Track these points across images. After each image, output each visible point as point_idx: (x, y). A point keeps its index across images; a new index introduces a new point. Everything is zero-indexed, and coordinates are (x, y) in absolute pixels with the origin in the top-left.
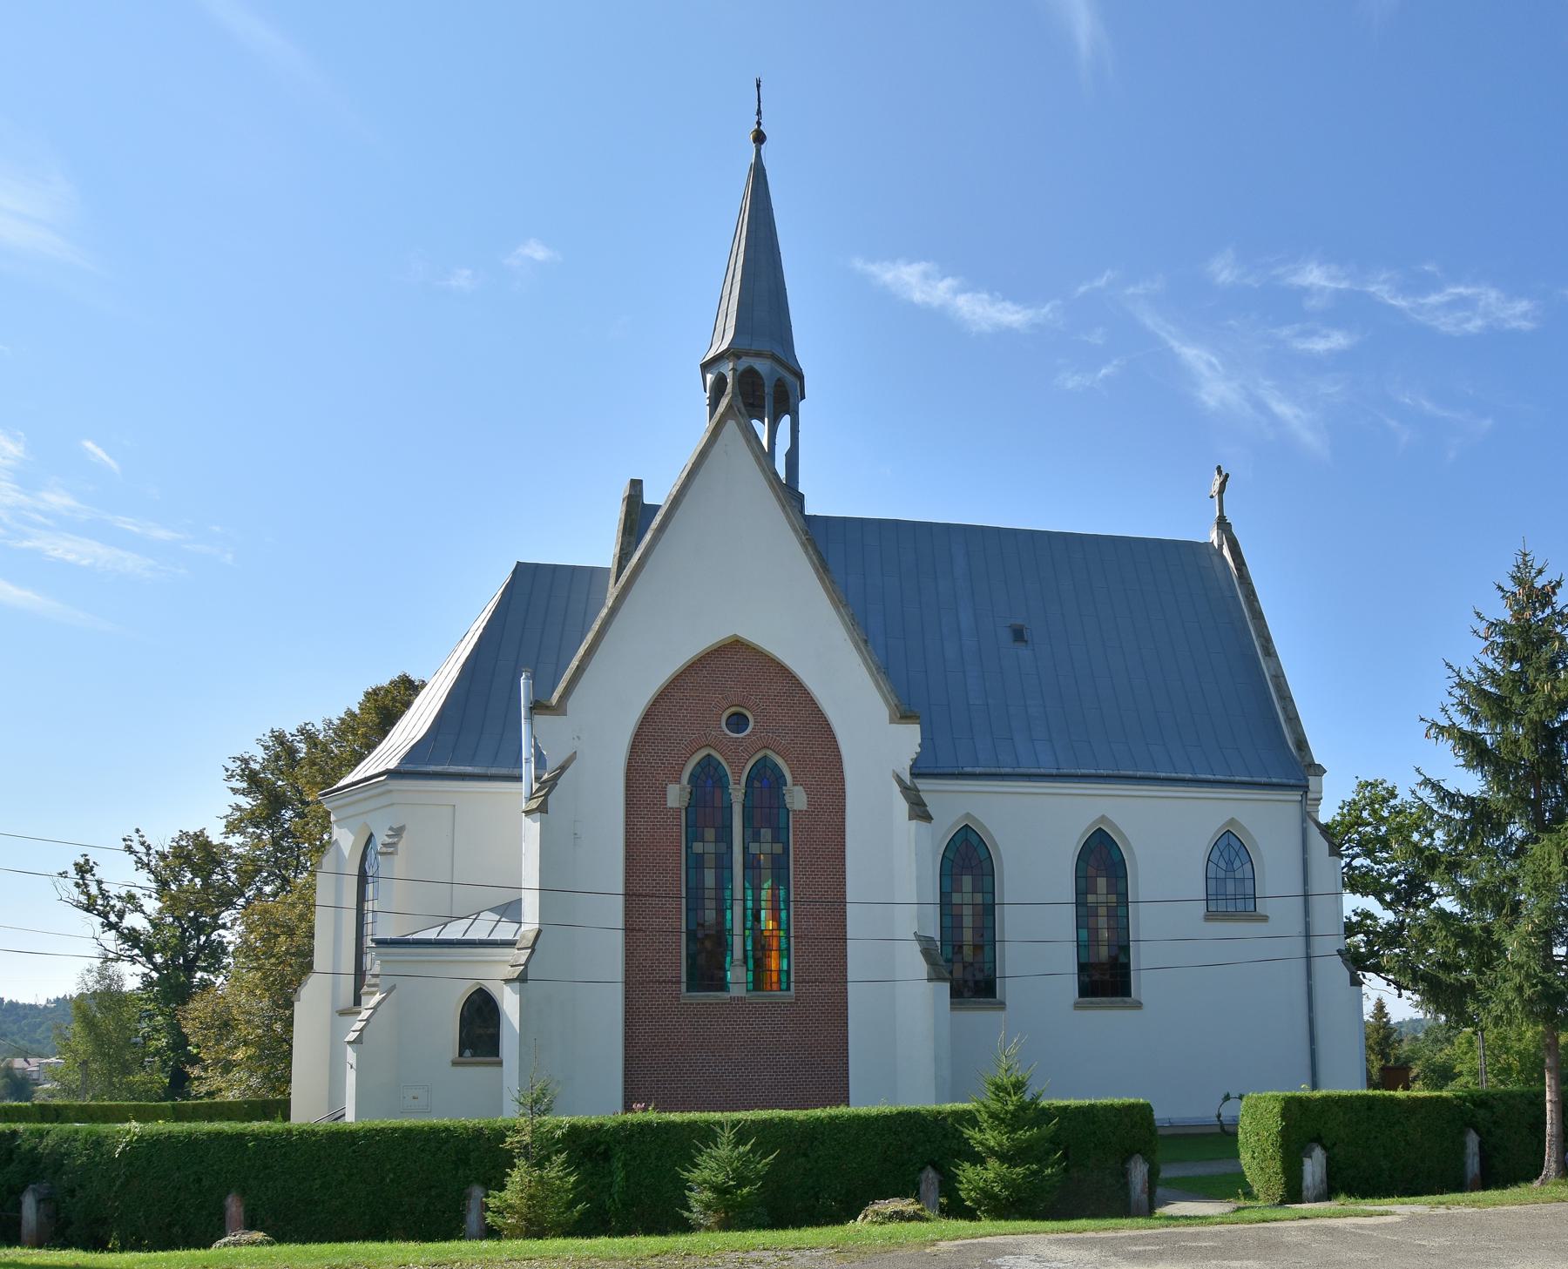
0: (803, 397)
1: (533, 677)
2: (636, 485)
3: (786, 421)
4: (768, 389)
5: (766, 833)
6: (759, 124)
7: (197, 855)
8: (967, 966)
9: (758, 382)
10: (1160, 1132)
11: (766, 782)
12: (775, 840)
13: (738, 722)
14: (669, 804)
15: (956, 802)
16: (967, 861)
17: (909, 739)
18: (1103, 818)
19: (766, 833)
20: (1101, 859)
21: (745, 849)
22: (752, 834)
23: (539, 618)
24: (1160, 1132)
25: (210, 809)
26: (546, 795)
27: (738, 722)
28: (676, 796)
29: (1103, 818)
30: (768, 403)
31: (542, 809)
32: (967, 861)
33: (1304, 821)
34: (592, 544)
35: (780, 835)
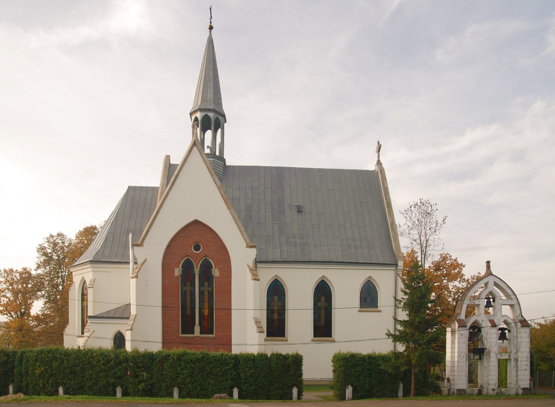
0: (226, 122)
2: (168, 158)
3: (220, 130)
4: (213, 120)
5: (206, 284)
6: (211, 22)
7: (26, 276)
8: (276, 327)
9: (210, 118)
11: (206, 268)
12: (209, 286)
13: (197, 248)
14: (176, 275)
15: (268, 274)
16: (276, 292)
17: (253, 253)
18: (324, 276)
19: (206, 284)
20: (323, 292)
21: (200, 289)
22: (201, 285)
23: (138, 206)
24: (305, 383)
25: (29, 260)
26: (138, 272)
27: (197, 248)
28: (178, 272)
29: (324, 276)
32: (276, 292)
33: (396, 277)
34: (154, 179)
35: (210, 284)
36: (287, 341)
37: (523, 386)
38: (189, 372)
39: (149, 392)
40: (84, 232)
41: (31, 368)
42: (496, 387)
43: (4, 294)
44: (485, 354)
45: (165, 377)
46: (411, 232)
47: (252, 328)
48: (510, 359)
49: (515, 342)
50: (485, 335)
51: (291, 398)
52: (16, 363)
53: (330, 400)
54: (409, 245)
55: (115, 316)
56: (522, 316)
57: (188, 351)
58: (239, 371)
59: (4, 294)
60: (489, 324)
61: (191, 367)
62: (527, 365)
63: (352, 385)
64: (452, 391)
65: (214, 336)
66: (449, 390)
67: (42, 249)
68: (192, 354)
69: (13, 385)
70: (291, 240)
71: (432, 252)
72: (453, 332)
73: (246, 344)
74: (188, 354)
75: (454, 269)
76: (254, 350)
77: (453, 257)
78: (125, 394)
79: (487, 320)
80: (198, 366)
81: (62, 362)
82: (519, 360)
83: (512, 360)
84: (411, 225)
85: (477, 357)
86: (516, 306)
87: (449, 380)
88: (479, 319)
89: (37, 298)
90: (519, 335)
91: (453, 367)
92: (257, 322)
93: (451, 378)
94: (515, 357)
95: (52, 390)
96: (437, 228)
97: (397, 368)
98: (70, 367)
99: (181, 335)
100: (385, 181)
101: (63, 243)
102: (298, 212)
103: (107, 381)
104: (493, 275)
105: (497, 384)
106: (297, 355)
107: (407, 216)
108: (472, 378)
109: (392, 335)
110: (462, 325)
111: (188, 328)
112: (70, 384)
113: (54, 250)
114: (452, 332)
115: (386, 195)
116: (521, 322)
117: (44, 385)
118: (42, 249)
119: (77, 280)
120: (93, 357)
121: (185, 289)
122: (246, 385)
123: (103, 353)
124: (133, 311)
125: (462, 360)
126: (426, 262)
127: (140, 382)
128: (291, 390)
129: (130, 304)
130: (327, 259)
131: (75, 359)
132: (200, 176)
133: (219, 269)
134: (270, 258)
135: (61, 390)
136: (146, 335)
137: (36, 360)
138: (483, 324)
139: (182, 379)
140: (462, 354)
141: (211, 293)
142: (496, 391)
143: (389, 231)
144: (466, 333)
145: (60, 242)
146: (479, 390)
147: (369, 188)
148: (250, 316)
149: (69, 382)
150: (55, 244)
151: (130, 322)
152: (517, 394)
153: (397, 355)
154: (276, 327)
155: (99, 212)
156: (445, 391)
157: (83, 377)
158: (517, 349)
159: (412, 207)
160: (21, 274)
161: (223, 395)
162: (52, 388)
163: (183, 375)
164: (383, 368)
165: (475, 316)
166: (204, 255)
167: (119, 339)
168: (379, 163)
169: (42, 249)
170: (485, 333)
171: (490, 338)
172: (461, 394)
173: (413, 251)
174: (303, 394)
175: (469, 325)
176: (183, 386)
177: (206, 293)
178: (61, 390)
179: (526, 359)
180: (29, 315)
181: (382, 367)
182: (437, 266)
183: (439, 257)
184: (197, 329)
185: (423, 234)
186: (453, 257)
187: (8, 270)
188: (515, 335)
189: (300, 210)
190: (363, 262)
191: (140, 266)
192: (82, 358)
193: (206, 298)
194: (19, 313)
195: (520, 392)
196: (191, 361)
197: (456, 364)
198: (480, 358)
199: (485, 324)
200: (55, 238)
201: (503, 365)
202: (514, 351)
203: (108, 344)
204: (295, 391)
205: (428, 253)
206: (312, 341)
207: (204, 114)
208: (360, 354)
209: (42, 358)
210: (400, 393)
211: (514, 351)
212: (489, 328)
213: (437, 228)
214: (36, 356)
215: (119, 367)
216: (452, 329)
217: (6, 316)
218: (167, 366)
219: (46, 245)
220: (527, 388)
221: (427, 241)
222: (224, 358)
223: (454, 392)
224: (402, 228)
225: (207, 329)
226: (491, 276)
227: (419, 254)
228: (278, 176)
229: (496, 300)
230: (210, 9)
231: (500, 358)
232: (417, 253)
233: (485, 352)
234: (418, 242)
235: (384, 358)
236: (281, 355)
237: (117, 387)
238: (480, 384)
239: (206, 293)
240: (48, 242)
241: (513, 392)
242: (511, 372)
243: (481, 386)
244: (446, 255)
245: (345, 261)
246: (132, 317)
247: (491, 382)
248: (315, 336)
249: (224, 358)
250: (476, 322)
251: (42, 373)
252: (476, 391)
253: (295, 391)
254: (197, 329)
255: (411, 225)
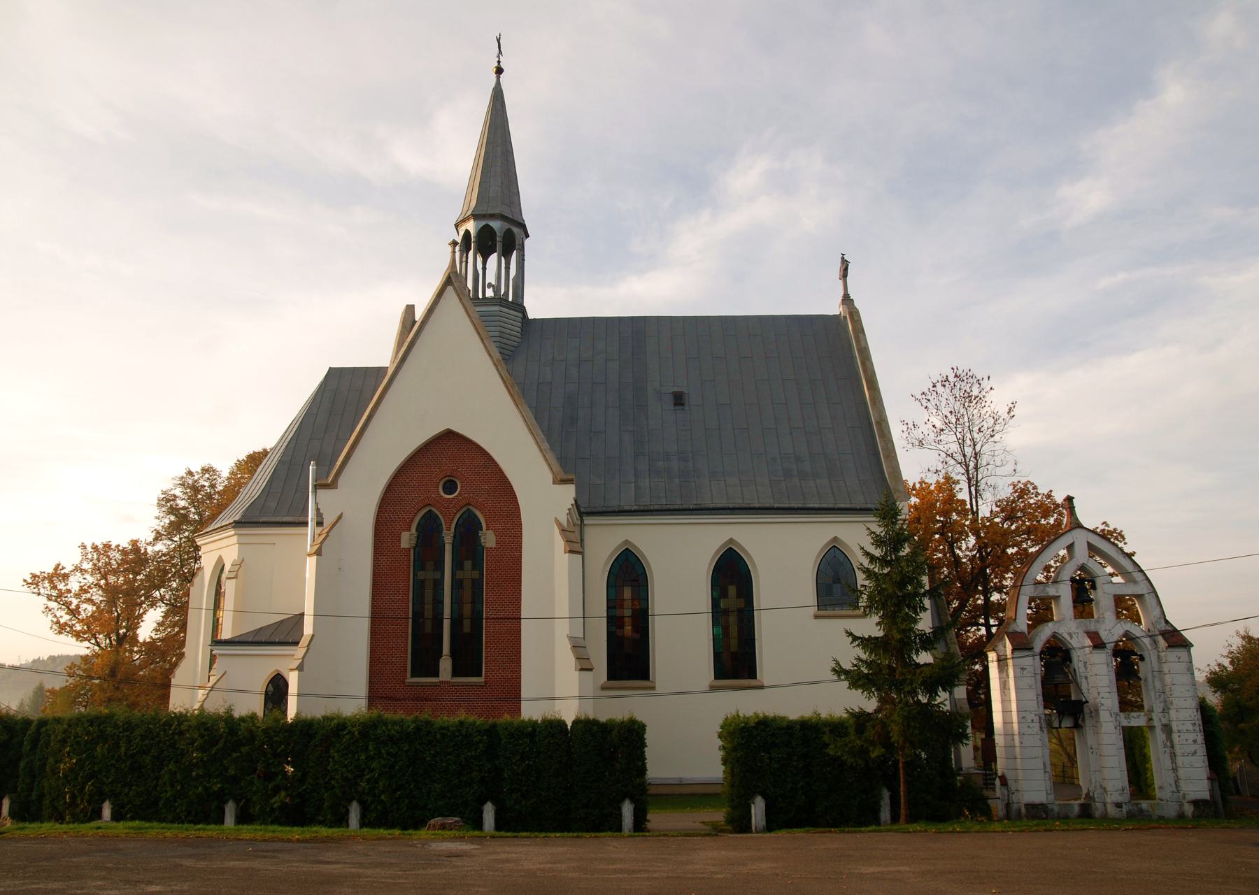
0: (527, 236)
1: (317, 464)
5: (468, 564)
7: (135, 557)
8: (628, 657)
9: (496, 227)
10: (652, 790)
11: (468, 532)
12: (474, 568)
13: (450, 487)
14: (403, 546)
15: (606, 539)
17: (568, 493)
18: (731, 540)
19: (468, 564)
20: (732, 574)
22: (457, 565)
23: (343, 401)
24: (652, 790)
25: (139, 524)
27: (450, 487)
28: (407, 540)
29: (731, 540)
30: (499, 246)
31: (318, 553)
32: (628, 574)
35: (477, 566)
36: (654, 688)
37: (1193, 796)
38: (384, 766)
39: (296, 815)
40: (246, 462)
41: (51, 760)
42: (1125, 797)
43: (88, 595)
44: (1087, 716)
45: (332, 778)
46: (942, 437)
47: (565, 659)
48: (1152, 728)
49: (1158, 685)
50: (1082, 669)
51: (619, 828)
52: (27, 747)
53: (723, 831)
54: (940, 467)
55: (272, 639)
56: (1167, 622)
57: (388, 715)
58: (497, 762)
59: (88, 595)
60: (1088, 642)
61: (389, 754)
62: (1195, 741)
63: (764, 796)
64: (1015, 807)
65: (481, 680)
66: (1008, 805)
67: (167, 502)
68: (395, 723)
69: (11, 799)
70: (661, 464)
71: (991, 481)
72: (1001, 661)
73: (553, 699)
74: (386, 724)
75: (1046, 516)
76: (568, 713)
77: (1043, 490)
78: (244, 818)
79: (1080, 631)
80: (407, 751)
81: (117, 745)
82: (1175, 728)
83: (1158, 730)
84: (939, 425)
85: (1067, 723)
86: (1147, 597)
87: (1004, 781)
88: (1063, 631)
89: (153, 605)
90: (1166, 668)
91: (1010, 747)
92: (578, 647)
93: (1009, 776)
94: (1164, 721)
95: (90, 809)
96: (997, 428)
97: (863, 752)
98: (133, 756)
99: (410, 680)
100: (861, 336)
101: (213, 486)
102: (675, 404)
103: (206, 789)
104: (1080, 526)
105: (1127, 791)
106: (633, 722)
107: (929, 404)
108: (1064, 776)
109: (846, 672)
110: (1022, 644)
111: (425, 663)
112: (127, 795)
113: (193, 500)
114: (999, 660)
115: (863, 364)
116: (1163, 634)
117: (73, 797)
118: (168, 501)
119: (207, 562)
120: (181, 733)
121: (421, 575)
122: (514, 796)
123: (203, 724)
124: (308, 629)
125: (1029, 731)
126: (980, 502)
127: (276, 790)
128: (620, 809)
129: (303, 614)
130: (738, 502)
131: (143, 737)
132: (461, 341)
133: (495, 530)
134: (614, 504)
135: (107, 811)
136: (333, 680)
137: (64, 741)
138: (1072, 642)
139: (368, 781)
140: (1030, 716)
141: (477, 585)
142: (1125, 808)
143: (874, 437)
144: (1033, 664)
145: (207, 484)
146: (1082, 805)
147: (826, 354)
148: (562, 631)
149: (126, 790)
150: (196, 489)
151: (299, 652)
152: (1181, 816)
153: (861, 719)
154: (628, 657)
155: (267, 424)
156: (997, 807)
157: (157, 778)
158: (1165, 701)
159: (939, 385)
160: (124, 552)
161: (450, 820)
162: (89, 804)
163: (372, 771)
164: (831, 753)
165: (1050, 624)
166: (464, 502)
167: (277, 690)
168: (847, 300)
169: (168, 501)
170: (1081, 665)
171: (1096, 677)
172: (1034, 817)
173: (948, 478)
174: (649, 817)
175: (1038, 646)
176: (370, 799)
177: (467, 585)
178: (107, 811)
179: (1191, 728)
180: (134, 639)
181: (831, 751)
182: (1009, 510)
183: (1010, 489)
184: (446, 665)
185: (968, 442)
186: (1043, 490)
187: (100, 546)
188: (1156, 669)
189: (679, 400)
190: (816, 506)
191: (329, 528)
192: (158, 734)
193: (467, 594)
194: (114, 637)
195: (1189, 810)
196: (391, 738)
197: (1017, 738)
198: (1077, 726)
199: (1078, 642)
200: (196, 477)
201: (1134, 743)
202: (1158, 707)
203: (251, 704)
204: (627, 809)
205: (982, 486)
206: (603, 688)
207: (483, 223)
208: (783, 719)
209: (77, 736)
210: (885, 814)
211: (1158, 707)
212: (1087, 650)
213: (997, 428)
214: (65, 731)
215: (235, 755)
216: (998, 656)
217: (86, 644)
218: (338, 751)
219: (178, 492)
220: (1204, 802)
221: (976, 455)
222: (464, 732)
223: (1019, 810)
224: (920, 431)
225: (467, 662)
226: (1077, 532)
227: (964, 485)
228: (633, 335)
229: (1098, 585)
230: (498, 41)
231: (1125, 723)
232: (958, 482)
233: (1086, 710)
234: (960, 458)
235: (836, 727)
236: (595, 722)
237: (227, 802)
238: (1084, 791)
239: (467, 585)
240: (183, 485)
241: (1171, 811)
242: (1158, 759)
243: (1088, 794)
244: (1025, 485)
245: (776, 506)
246: (304, 642)
247: (1110, 786)
248: (716, 678)
249: (464, 732)
250: (1054, 635)
251: (71, 770)
252: (1077, 809)
253: (627, 809)
254: (446, 665)
255: (939, 425)
